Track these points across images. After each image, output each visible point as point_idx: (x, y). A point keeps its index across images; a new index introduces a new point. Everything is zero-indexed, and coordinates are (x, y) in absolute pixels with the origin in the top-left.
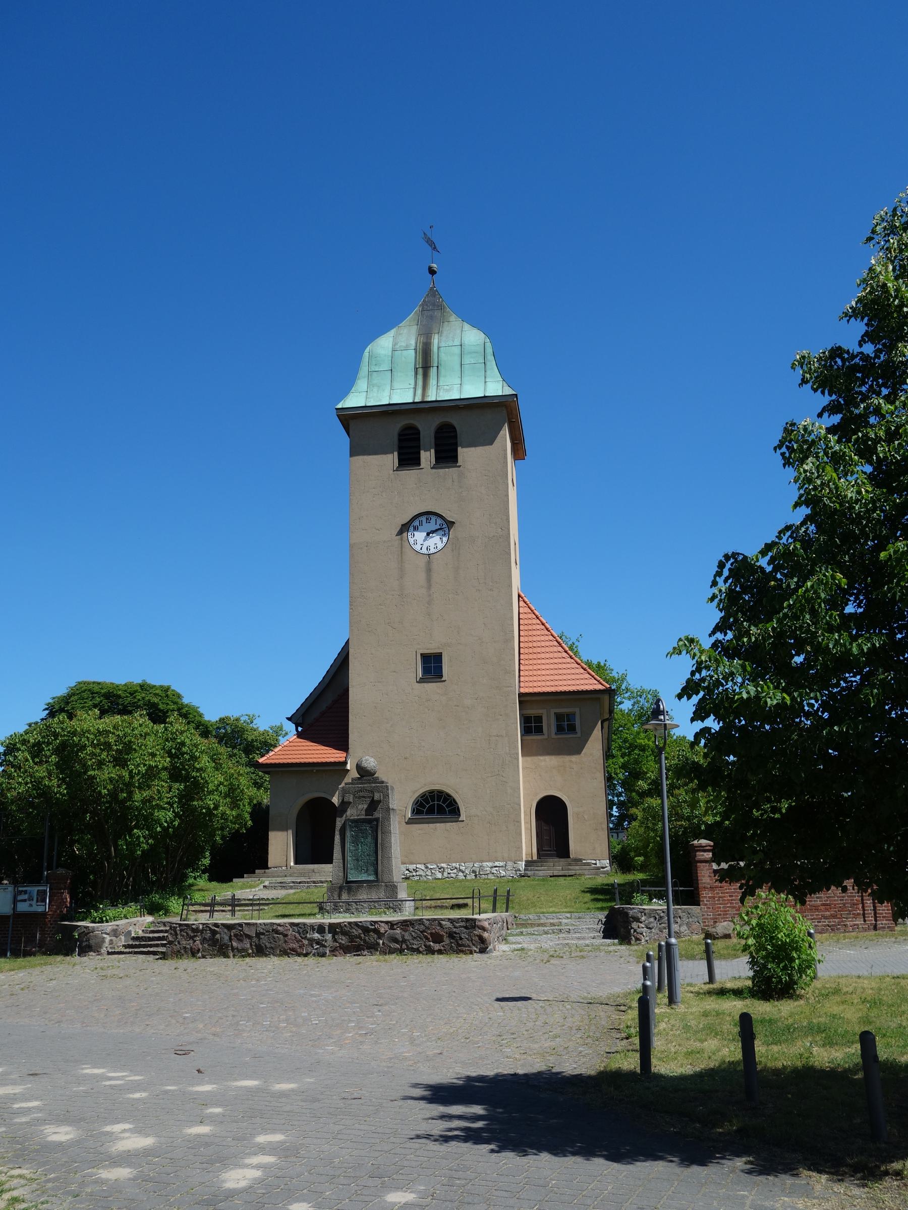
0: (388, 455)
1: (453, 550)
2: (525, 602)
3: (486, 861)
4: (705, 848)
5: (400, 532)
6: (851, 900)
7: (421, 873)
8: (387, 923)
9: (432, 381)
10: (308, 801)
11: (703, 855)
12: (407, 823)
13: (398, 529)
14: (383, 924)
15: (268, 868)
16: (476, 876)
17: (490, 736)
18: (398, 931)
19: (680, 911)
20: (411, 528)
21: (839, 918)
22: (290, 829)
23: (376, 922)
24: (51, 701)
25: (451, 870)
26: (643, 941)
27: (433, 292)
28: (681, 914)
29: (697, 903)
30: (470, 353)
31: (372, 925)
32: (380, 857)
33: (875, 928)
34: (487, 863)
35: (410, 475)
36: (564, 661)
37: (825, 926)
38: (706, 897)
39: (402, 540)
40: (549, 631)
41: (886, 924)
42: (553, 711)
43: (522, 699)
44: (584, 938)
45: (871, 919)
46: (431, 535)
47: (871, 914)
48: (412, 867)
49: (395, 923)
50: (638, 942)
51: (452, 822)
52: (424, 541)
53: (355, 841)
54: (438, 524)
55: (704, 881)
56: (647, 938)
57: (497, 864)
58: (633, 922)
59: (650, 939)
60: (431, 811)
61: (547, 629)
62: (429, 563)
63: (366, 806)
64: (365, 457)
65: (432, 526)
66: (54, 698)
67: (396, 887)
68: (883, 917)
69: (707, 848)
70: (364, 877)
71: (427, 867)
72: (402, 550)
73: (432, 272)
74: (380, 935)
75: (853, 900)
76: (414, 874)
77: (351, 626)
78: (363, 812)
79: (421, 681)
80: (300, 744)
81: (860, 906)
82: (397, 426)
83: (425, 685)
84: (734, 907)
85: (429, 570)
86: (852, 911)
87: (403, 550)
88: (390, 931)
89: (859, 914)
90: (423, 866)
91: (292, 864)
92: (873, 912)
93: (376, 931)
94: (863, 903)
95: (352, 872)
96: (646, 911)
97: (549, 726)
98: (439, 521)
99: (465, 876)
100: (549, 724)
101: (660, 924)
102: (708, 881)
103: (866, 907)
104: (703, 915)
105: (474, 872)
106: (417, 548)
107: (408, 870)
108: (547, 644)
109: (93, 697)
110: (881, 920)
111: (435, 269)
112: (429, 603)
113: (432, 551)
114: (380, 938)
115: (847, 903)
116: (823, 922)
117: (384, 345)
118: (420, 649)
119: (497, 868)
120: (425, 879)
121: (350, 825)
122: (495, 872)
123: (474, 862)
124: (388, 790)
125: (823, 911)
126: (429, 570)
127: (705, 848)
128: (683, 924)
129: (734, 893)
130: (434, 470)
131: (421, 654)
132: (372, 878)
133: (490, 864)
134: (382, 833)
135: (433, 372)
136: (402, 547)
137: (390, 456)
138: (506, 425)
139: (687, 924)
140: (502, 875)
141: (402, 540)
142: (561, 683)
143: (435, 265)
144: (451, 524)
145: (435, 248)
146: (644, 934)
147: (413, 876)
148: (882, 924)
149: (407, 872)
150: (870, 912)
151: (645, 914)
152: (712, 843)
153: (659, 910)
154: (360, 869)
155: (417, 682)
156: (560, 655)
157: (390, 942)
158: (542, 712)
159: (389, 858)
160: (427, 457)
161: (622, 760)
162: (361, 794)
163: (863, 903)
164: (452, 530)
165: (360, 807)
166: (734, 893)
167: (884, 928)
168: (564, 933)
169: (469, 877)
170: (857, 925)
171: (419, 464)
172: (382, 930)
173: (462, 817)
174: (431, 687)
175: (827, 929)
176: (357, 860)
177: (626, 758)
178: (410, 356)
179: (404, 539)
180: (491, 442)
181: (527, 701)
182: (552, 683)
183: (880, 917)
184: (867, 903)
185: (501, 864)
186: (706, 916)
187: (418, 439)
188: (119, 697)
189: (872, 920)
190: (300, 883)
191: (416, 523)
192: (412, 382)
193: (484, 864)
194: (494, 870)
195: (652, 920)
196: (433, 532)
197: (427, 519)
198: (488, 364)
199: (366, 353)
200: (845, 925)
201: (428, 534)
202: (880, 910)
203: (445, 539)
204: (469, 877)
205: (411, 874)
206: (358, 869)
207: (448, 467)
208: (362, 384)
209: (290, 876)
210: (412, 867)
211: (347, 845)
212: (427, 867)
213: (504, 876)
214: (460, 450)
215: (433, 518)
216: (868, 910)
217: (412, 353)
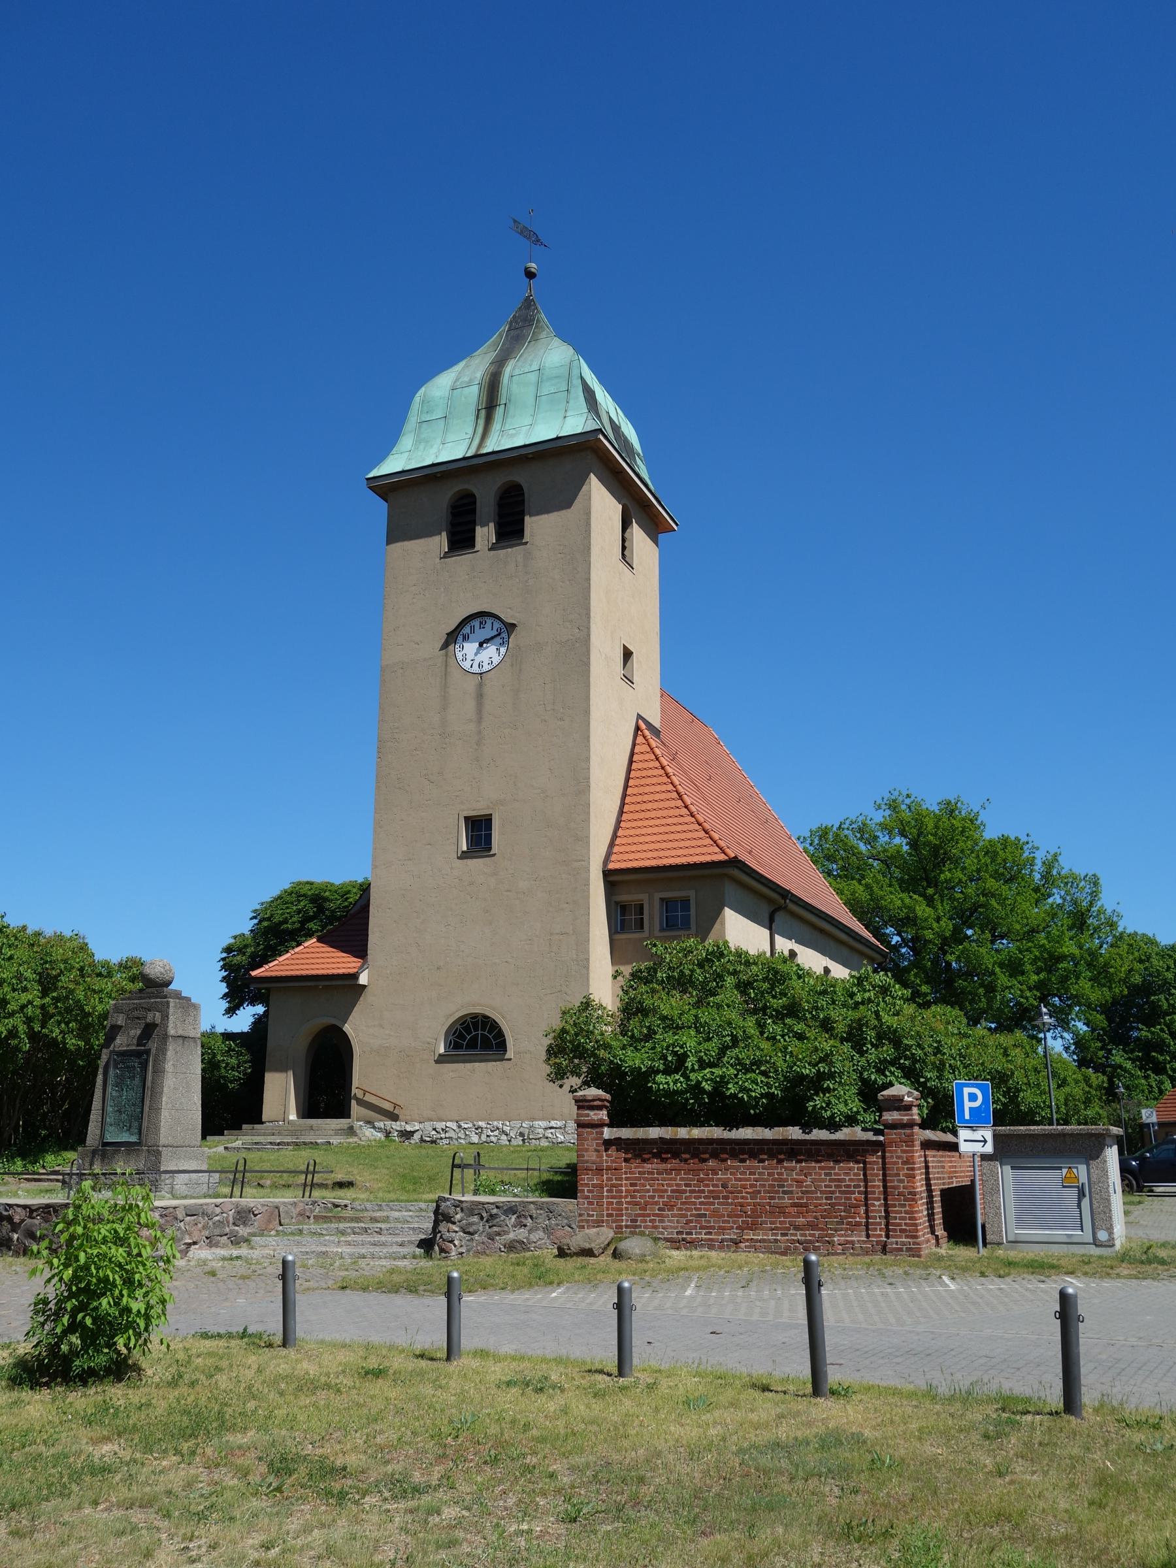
0: (434, 538)
1: (512, 665)
2: (645, 737)
3: (539, 1120)
4: (592, 1103)
5: (445, 646)
6: (847, 1199)
7: (451, 1134)
8: (25, 1207)
9: (496, 426)
10: (320, 1031)
11: (588, 1115)
12: (437, 1062)
13: (443, 641)
14: (19, 1210)
15: (262, 1123)
16: (523, 1140)
17: (551, 934)
18: (37, 1221)
19: (532, 1206)
20: (460, 638)
21: (822, 1229)
22: (290, 1069)
23: (10, 1206)
24: (258, 907)
25: (492, 1131)
26: (453, 1254)
27: (528, 303)
28: (534, 1212)
29: (573, 1196)
30: (550, 379)
31: (6, 1210)
32: (146, 1109)
33: (884, 1250)
34: (540, 1123)
35: (463, 560)
36: (681, 820)
37: (793, 1242)
38: (587, 1185)
39: (447, 655)
40: (669, 777)
41: (903, 1244)
42: (658, 896)
43: (612, 878)
44: (384, 1244)
45: (879, 1233)
46: (485, 645)
47: (880, 1224)
48: (440, 1125)
49: (34, 1208)
50: (443, 1255)
51: (495, 1061)
52: (476, 654)
53: (119, 1085)
54: (495, 629)
55: (586, 1158)
56: (461, 1250)
57: (553, 1124)
58: (442, 1221)
59: (468, 1251)
60: (472, 1045)
61: (667, 775)
62: (480, 686)
63: (139, 1032)
64: (406, 543)
65: (488, 632)
66: (262, 904)
67: (159, 1153)
68: (901, 1231)
69: (596, 1103)
70: (125, 1137)
71: (460, 1127)
72: (446, 670)
73: (530, 275)
74: (15, 1227)
75: (849, 1199)
76: (443, 1136)
77: (378, 782)
78: (135, 1041)
79: (464, 856)
80: (318, 950)
81: (862, 1210)
82: (445, 496)
83: (469, 861)
84: (637, 1204)
85: (480, 696)
86: (847, 1217)
87: (449, 670)
88: (28, 1221)
89: (858, 1224)
90: (455, 1124)
91: (293, 1117)
92: (883, 1222)
93: (10, 1219)
94: (866, 1205)
95: (111, 1129)
96: (464, 1205)
97: (651, 918)
98: (497, 625)
99: (509, 1141)
100: (653, 914)
101: (490, 1227)
102: (594, 1158)
103: (873, 1211)
104: (580, 1215)
105: (522, 1134)
106: (466, 665)
107: (434, 1129)
108: (663, 796)
109: (299, 901)
110: (896, 1237)
111: (533, 270)
112: (478, 743)
113: (486, 668)
114: (14, 1230)
115: (840, 1204)
116: (792, 1235)
117: (441, 385)
118: (463, 810)
119: (553, 1131)
120: (456, 1142)
121: (115, 1060)
122: (550, 1135)
123: (523, 1121)
124: (168, 1007)
125: (794, 1217)
126: (480, 696)
127: (592, 1103)
128: (537, 1229)
129: (639, 1179)
130: (492, 553)
131: (466, 818)
132: (134, 1139)
133: (543, 1124)
134: (154, 1072)
135: (499, 411)
136: (446, 666)
137: (437, 539)
138: (594, 480)
139: (546, 1229)
140: (559, 1140)
141: (447, 655)
142: (667, 853)
143: (533, 265)
144: (511, 627)
145: (538, 241)
146: (456, 1242)
147: (441, 1139)
148: (897, 1244)
149: (434, 1132)
150: (878, 1220)
151: (462, 1210)
152: (608, 1097)
153: (488, 1203)
154: (121, 1125)
155: (458, 858)
156: (677, 812)
157: (26, 1237)
158: (643, 897)
159: (157, 1110)
160: (485, 534)
161: (1035, 978)
162: (136, 1013)
163: (866, 1205)
164: (512, 636)
165: (132, 1033)
166: (639, 1179)
167: (901, 1250)
168: (371, 1234)
169: (514, 1142)
170: (852, 1242)
171: (473, 546)
172: (17, 1219)
173: (510, 1054)
174: (476, 864)
175: (796, 1248)
176: (119, 1111)
177: (1042, 975)
178: (472, 394)
179: (449, 654)
180: (567, 504)
181: (622, 882)
182: (655, 854)
183: (895, 1230)
184: (874, 1205)
185: (559, 1124)
186: (585, 1217)
187: (474, 511)
188: (326, 899)
189: (880, 1236)
190: (279, 1144)
191: (466, 630)
192: (470, 431)
193: (536, 1123)
194: (548, 1133)
195: (475, 1219)
196: (487, 641)
197: (481, 623)
198: (572, 390)
199: (417, 399)
200: (829, 1242)
201: (481, 645)
202: (895, 1218)
203: (503, 650)
204: (514, 1142)
205: (439, 1136)
206: (120, 1125)
207: (511, 546)
208: (406, 441)
209: (280, 1134)
210: (440, 1125)
211: (109, 1089)
212: (460, 1127)
213: (561, 1143)
214: (527, 519)
215: (489, 621)
216: (875, 1218)
217: (475, 390)
